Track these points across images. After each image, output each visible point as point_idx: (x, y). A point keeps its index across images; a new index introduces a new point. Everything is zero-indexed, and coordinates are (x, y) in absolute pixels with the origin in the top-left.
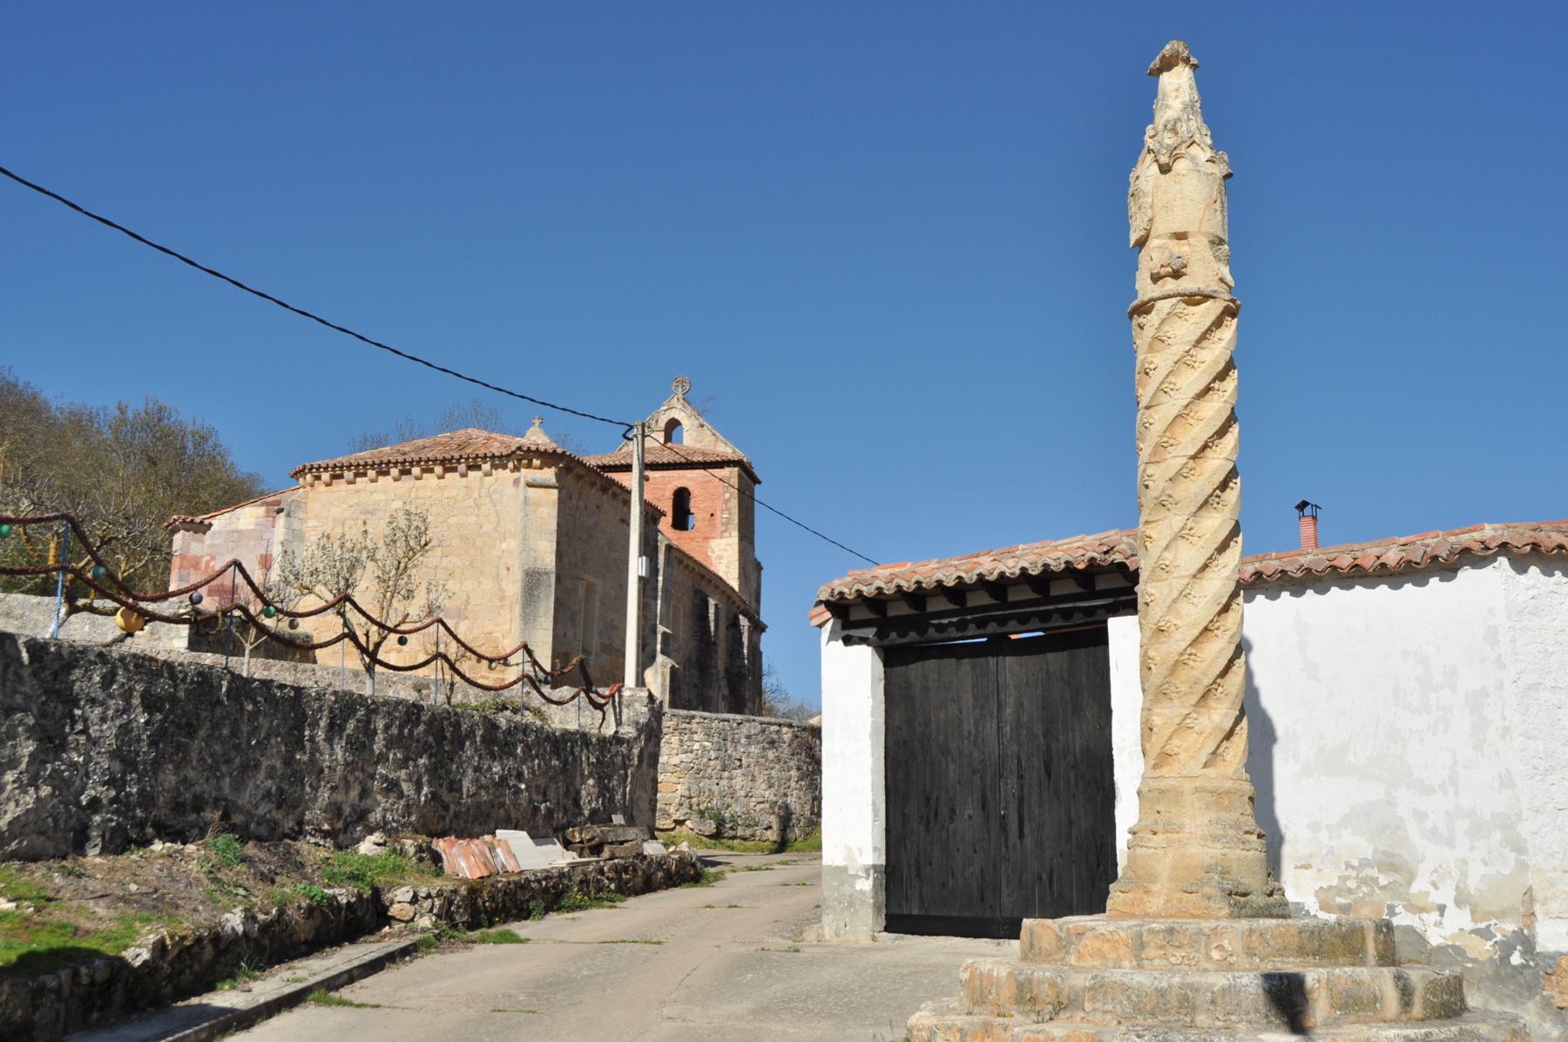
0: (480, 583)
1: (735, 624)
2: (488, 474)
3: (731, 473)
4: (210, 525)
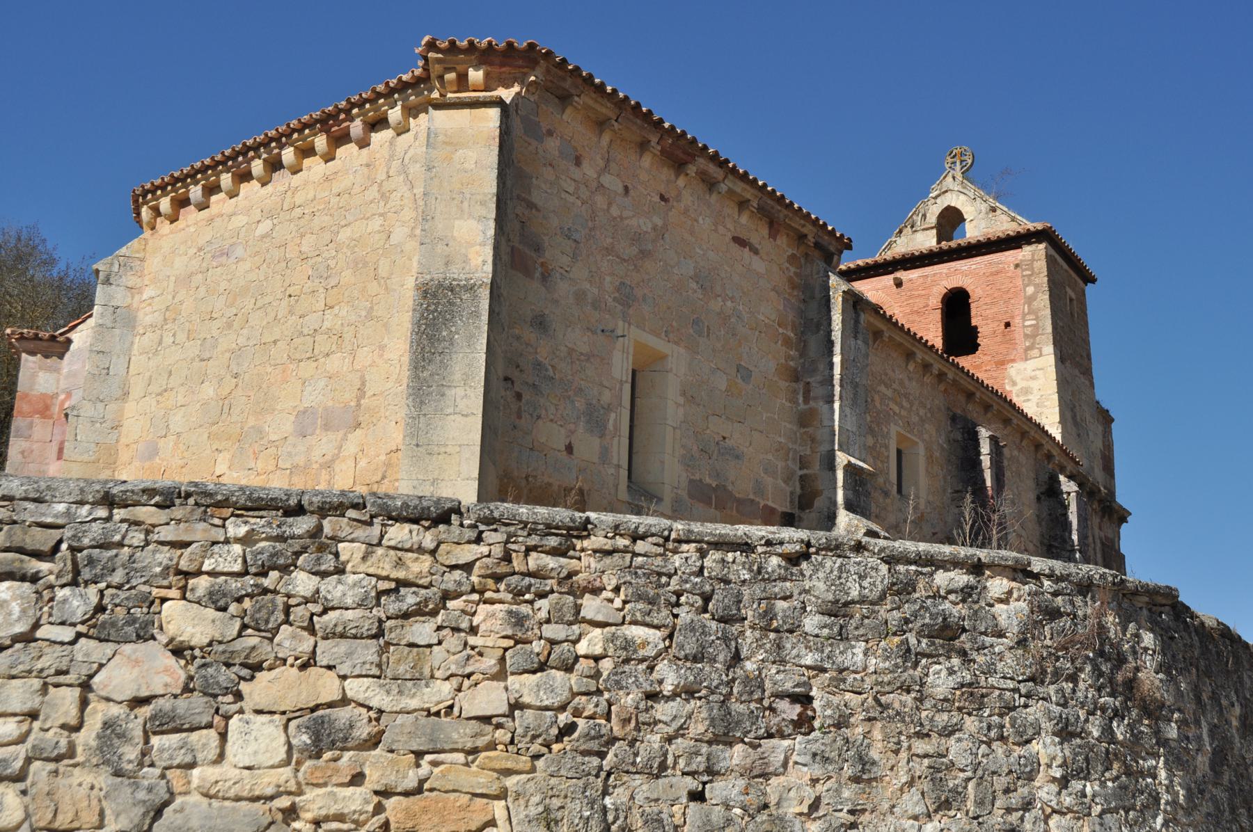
0: (382, 348)
1: (1052, 491)
2: (402, 130)
3: (1036, 253)
4: (69, 341)
